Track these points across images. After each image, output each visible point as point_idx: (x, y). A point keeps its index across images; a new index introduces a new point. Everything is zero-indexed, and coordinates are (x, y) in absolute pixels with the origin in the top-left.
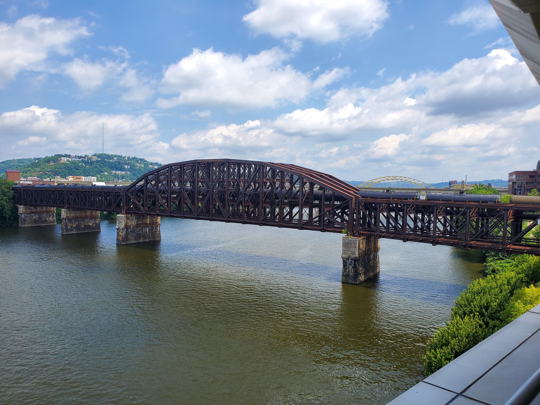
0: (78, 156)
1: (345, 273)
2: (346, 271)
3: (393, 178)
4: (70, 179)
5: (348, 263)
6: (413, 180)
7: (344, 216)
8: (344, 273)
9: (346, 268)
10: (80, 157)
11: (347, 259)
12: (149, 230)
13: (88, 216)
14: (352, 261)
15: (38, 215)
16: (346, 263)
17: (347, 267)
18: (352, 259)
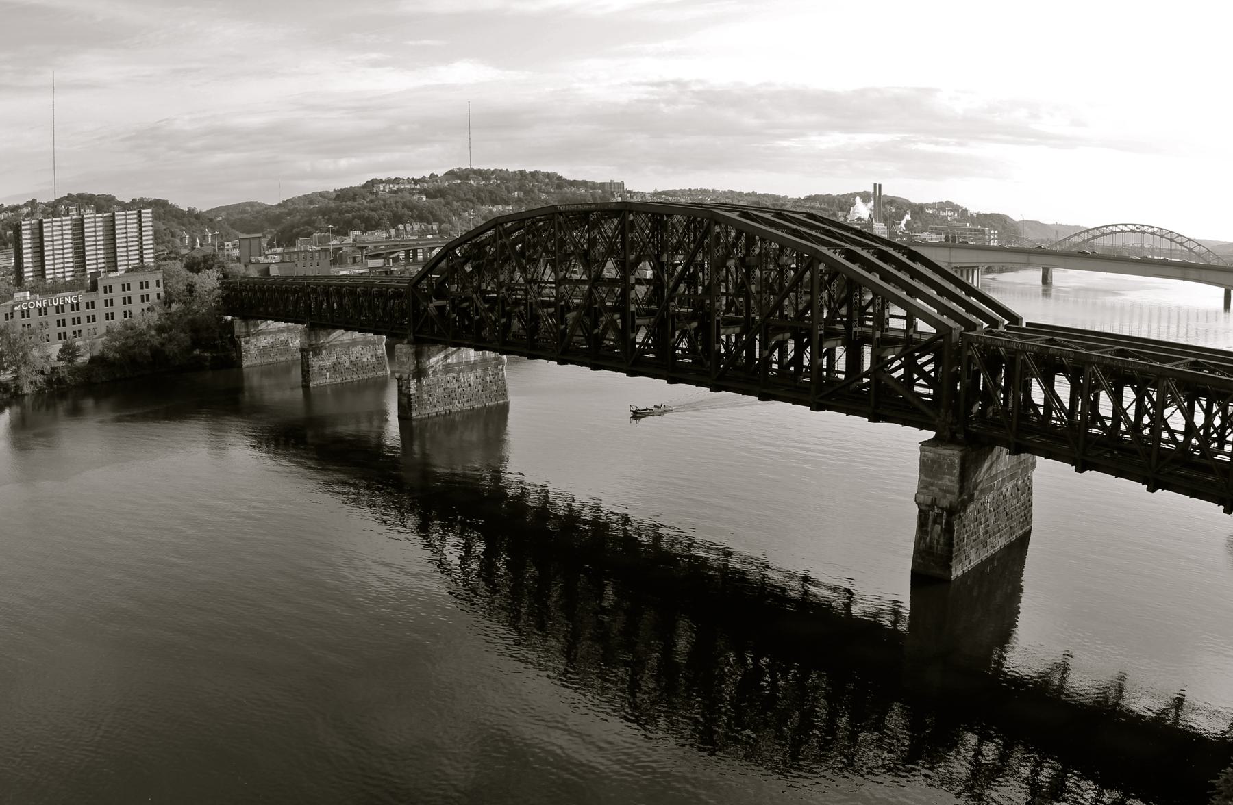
0: (413, 179)
1: (921, 545)
2: (925, 539)
3: (1134, 228)
4: (511, 208)
6: (1177, 237)
8: (919, 544)
9: (926, 530)
10: (416, 181)
11: (929, 506)
12: (477, 378)
13: (358, 340)
14: (942, 515)
15: (272, 338)
16: (925, 517)
17: (929, 529)
18: (942, 509)
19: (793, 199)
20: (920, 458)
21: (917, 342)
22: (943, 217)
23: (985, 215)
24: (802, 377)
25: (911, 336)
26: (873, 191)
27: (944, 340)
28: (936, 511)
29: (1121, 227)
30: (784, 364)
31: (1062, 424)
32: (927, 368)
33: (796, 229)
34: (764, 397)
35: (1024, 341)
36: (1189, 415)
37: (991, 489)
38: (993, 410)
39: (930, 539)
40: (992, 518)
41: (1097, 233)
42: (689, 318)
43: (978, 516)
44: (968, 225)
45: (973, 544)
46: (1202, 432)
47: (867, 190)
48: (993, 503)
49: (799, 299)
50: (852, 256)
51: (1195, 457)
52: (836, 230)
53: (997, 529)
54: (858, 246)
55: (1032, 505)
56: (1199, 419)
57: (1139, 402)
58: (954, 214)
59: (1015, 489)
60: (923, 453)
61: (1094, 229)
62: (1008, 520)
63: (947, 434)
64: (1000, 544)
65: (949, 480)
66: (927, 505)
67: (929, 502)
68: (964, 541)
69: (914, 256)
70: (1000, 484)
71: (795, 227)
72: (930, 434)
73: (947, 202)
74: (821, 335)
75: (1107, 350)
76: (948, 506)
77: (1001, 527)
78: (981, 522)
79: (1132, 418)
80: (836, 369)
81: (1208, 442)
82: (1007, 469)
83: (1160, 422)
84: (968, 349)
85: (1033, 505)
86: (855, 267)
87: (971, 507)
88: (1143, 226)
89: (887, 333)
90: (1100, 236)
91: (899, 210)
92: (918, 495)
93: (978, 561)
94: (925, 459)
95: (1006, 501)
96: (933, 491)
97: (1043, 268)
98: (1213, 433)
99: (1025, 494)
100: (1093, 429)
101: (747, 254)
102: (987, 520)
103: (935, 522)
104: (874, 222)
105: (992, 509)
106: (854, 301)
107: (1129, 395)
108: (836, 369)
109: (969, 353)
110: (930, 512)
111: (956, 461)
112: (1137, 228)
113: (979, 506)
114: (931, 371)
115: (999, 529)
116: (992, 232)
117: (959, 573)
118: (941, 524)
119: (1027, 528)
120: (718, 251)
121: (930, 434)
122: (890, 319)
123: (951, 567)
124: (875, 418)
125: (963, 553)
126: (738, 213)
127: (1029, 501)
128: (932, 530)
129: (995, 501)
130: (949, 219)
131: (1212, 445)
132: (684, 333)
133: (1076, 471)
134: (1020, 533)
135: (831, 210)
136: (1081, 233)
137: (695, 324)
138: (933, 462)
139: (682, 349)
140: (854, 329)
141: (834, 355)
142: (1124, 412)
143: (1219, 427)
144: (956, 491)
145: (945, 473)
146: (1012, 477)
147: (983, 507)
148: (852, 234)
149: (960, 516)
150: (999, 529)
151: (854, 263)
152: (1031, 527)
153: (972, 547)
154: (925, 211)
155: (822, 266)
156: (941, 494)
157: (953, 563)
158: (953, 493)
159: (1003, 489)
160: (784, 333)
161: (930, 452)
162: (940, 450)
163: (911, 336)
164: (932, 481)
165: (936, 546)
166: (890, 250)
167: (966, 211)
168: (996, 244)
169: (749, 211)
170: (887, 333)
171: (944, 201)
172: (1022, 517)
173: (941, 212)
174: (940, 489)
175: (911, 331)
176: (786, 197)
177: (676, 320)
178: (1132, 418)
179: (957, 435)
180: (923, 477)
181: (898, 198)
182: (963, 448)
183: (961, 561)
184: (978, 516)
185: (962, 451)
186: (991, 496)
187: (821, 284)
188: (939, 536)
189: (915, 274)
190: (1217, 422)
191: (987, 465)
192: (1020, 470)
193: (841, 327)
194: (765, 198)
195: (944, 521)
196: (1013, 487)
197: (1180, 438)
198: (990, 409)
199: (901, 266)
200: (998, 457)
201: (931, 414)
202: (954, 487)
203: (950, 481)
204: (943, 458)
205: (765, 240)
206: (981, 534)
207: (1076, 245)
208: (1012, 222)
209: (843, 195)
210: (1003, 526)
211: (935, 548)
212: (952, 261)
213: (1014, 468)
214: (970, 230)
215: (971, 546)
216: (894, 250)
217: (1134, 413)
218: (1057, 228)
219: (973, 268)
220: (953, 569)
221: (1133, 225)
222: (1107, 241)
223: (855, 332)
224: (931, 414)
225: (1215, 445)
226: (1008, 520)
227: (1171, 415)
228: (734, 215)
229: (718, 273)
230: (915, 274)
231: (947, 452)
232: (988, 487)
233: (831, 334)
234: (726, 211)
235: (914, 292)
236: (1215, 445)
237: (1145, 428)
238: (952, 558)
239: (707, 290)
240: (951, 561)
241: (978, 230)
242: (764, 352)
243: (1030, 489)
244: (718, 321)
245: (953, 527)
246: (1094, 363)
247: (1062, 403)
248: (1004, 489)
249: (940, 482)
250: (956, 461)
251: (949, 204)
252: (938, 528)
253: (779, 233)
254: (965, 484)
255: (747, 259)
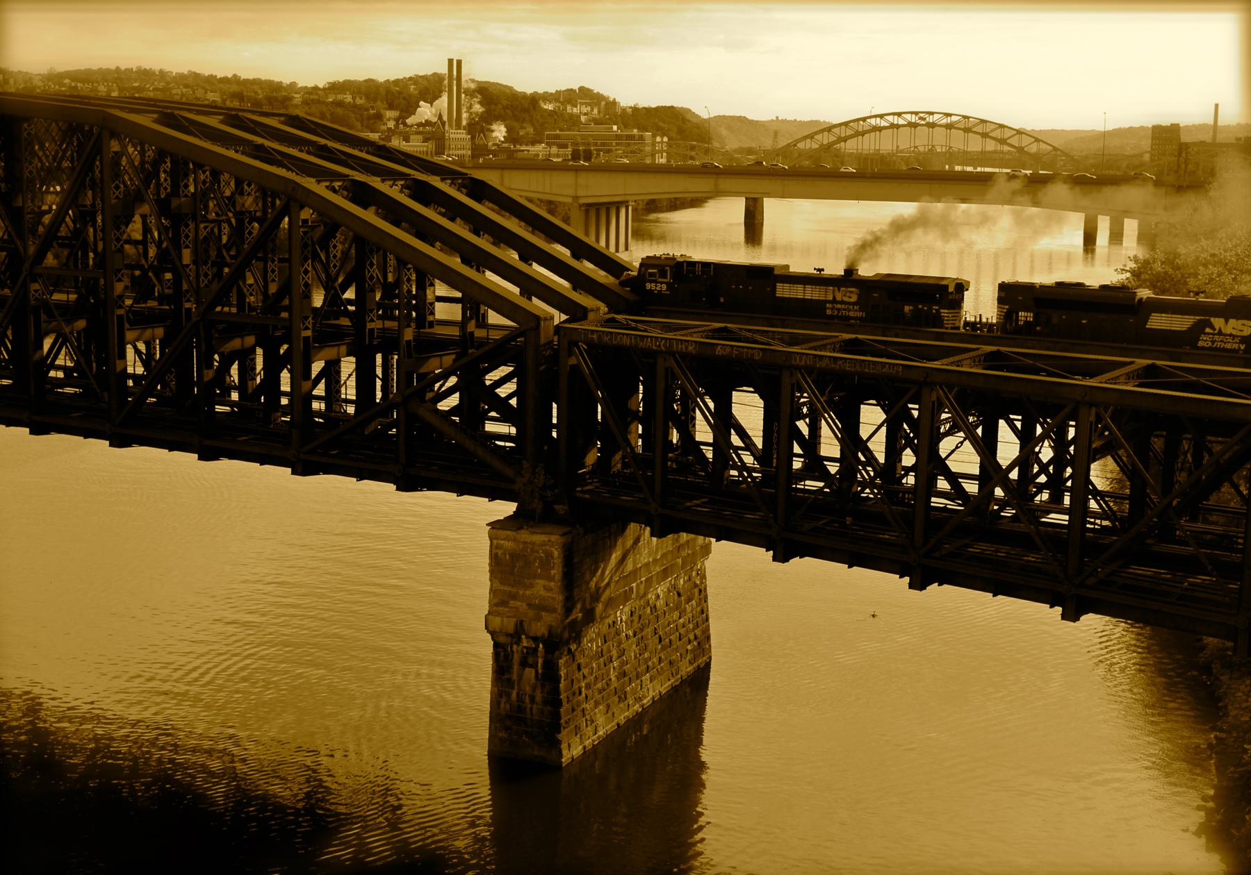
1: (502, 705)
2: (509, 695)
3: (914, 119)
5: (516, 658)
7: (513, 381)
8: (499, 703)
11: (511, 635)
14: (536, 650)
17: (515, 677)
18: (535, 639)
19: (306, 87)
20: (491, 551)
21: (483, 342)
22: (571, 116)
23: (648, 110)
24: (279, 414)
25: (472, 333)
26: (446, 72)
27: (525, 339)
28: (525, 644)
29: (890, 118)
30: (250, 391)
31: (741, 475)
32: (503, 391)
33: (262, 145)
34: (208, 454)
35: (670, 335)
36: (987, 447)
37: (626, 597)
38: (623, 457)
39: (518, 694)
40: (632, 651)
41: (844, 132)
42: (70, 313)
43: (605, 647)
44: (615, 128)
45: (598, 697)
46: (1014, 475)
47: (439, 72)
48: (632, 622)
49: (270, 274)
50: (363, 195)
51: (1005, 521)
52: (337, 146)
53: (644, 667)
54: (434, 174)
55: (707, 620)
56: (1008, 448)
57: (893, 425)
58: (592, 110)
59: (674, 594)
60: (495, 542)
61: (841, 125)
62: (663, 648)
63: (537, 505)
64: (651, 693)
65: (545, 588)
66: (507, 635)
67: (511, 629)
68: (580, 693)
69: (479, 190)
70: (642, 587)
71: (260, 141)
72: (506, 508)
73: (581, 89)
74: (306, 339)
75: (825, 342)
76: (546, 634)
77: (650, 663)
78: (611, 657)
79: (881, 458)
80: (343, 396)
81: (1027, 490)
82: (655, 560)
83: (933, 465)
84: (570, 353)
85: (710, 620)
86: (369, 215)
87: (592, 632)
88: (932, 113)
89: (430, 330)
90: (851, 137)
91: (493, 106)
92: (490, 617)
93: (611, 727)
94: (500, 552)
95: (657, 617)
96: (517, 608)
97: (746, 199)
98: (1038, 474)
99: (694, 602)
100: (808, 482)
101: (175, 192)
102: (622, 653)
103: (524, 664)
104: (447, 127)
105: (631, 633)
106: (368, 276)
107: (871, 416)
108: (343, 396)
109: (573, 361)
110: (515, 647)
111: (556, 553)
112: (920, 118)
113: (605, 629)
114: (510, 396)
115: (648, 667)
116: (658, 139)
117: (577, 751)
118: (534, 666)
119: (701, 661)
120: (117, 187)
121: (506, 508)
122: (437, 304)
123: (559, 742)
124: (407, 484)
125: (580, 714)
126: (221, 117)
127: (702, 612)
128: (520, 677)
129: (636, 618)
130: (583, 119)
131: (1038, 498)
132: (62, 340)
133: (774, 560)
134: (686, 669)
135: (373, 108)
136: (817, 133)
137: (81, 324)
138: (514, 556)
139: (63, 368)
140: (370, 326)
141: (338, 373)
142: (863, 445)
143: (1049, 463)
144: (559, 607)
145: (535, 576)
146: (665, 573)
147: (613, 630)
148: (368, 152)
149: (570, 650)
150: (648, 667)
151: (365, 206)
152: (710, 658)
153: (597, 704)
154: (540, 106)
155: (306, 214)
156: (531, 613)
157: (563, 735)
158: (554, 610)
159: (650, 596)
160: (242, 337)
161: (507, 539)
162: (525, 536)
163: (472, 333)
164: (514, 590)
165: (529, 706)
166: (435, 181)
167: (614, 103)
168: (663, 161)
169: (176, 112)
170: (430, 330)
171: (576, 87)
172: (690, 641)
173: (569, 107)
174: (529, 605)
175: (471, 326)
176: (293, 84)
177: (43, 317)
178: (881, 458)
179: (557, 507)
180: (497, 585)
181: (493, 84)
182: (567, 529)
183: (577, 729)
184: (605, 647)
185: (564, 535)
186: (627, 609)
187: (305, 246)
188: (534, 689)
189: (480, 225)
190: (1046, 453)
191: (615, 556)
192: (680, 561)
193: (345, 322)
194: (256, 87)
195: (540, 661)
196: (669, 591)
197: (972, 488)
198: (618, 456)
199: (454, 210)
200: (637, 541)
201: (509, 472)
202: (553, 598)
203: (547, 588)
204: (532, 549)
205: (204, 166)
206: (613, 679)
207: (810, 154)
208: (695, 120)
209: (397, 82)
210: (655, 660)
211: (528, 710)
212: (580, 193)
213: (670, 557)
214: (618, 137)
215: (595, 701)
216: (442, 180)
217: (883, 448)
218: (775, 127)
219: (618, 205)
220: (564, 746)
221: (912, 113)
222: (867, 145)
223: (372, 330)
224: (509, 472)
225: (1045, 496)
226: (663, 648)
227: (957, 447)
228: (146, 120)
229: (118, 229)
230: (480, 225)
231: (538, 538)
232: (620, 594)
233: (327, 336)
234: (131, 111)
235: (529, 253)
236: (1045, 496)
237: (906, 475)
238: (559, 725)
239: (101, 260)
240: (559, 732)
241: (631, 137)
242: (206, 371)
243: (702, 591)
244: (120, 317)
245: (558, 670)
246: (798, 368)
247: (749, 437)
248: (652, 596)
249: (527, 592)
250: (556, 553)
251: (585, 93)
252: (530, 673)
253: (231, 154)
254: (576, 592)
255: (175, 203)
